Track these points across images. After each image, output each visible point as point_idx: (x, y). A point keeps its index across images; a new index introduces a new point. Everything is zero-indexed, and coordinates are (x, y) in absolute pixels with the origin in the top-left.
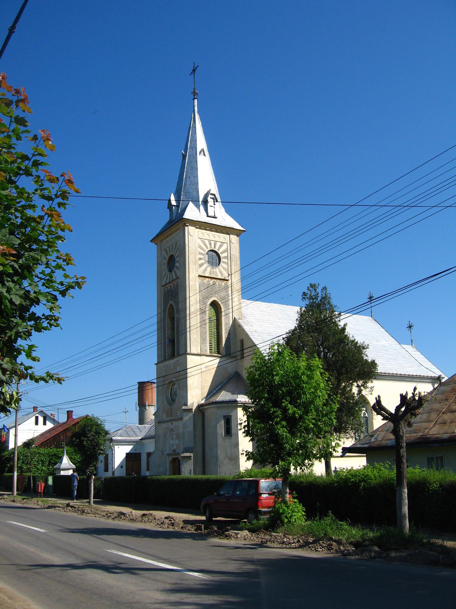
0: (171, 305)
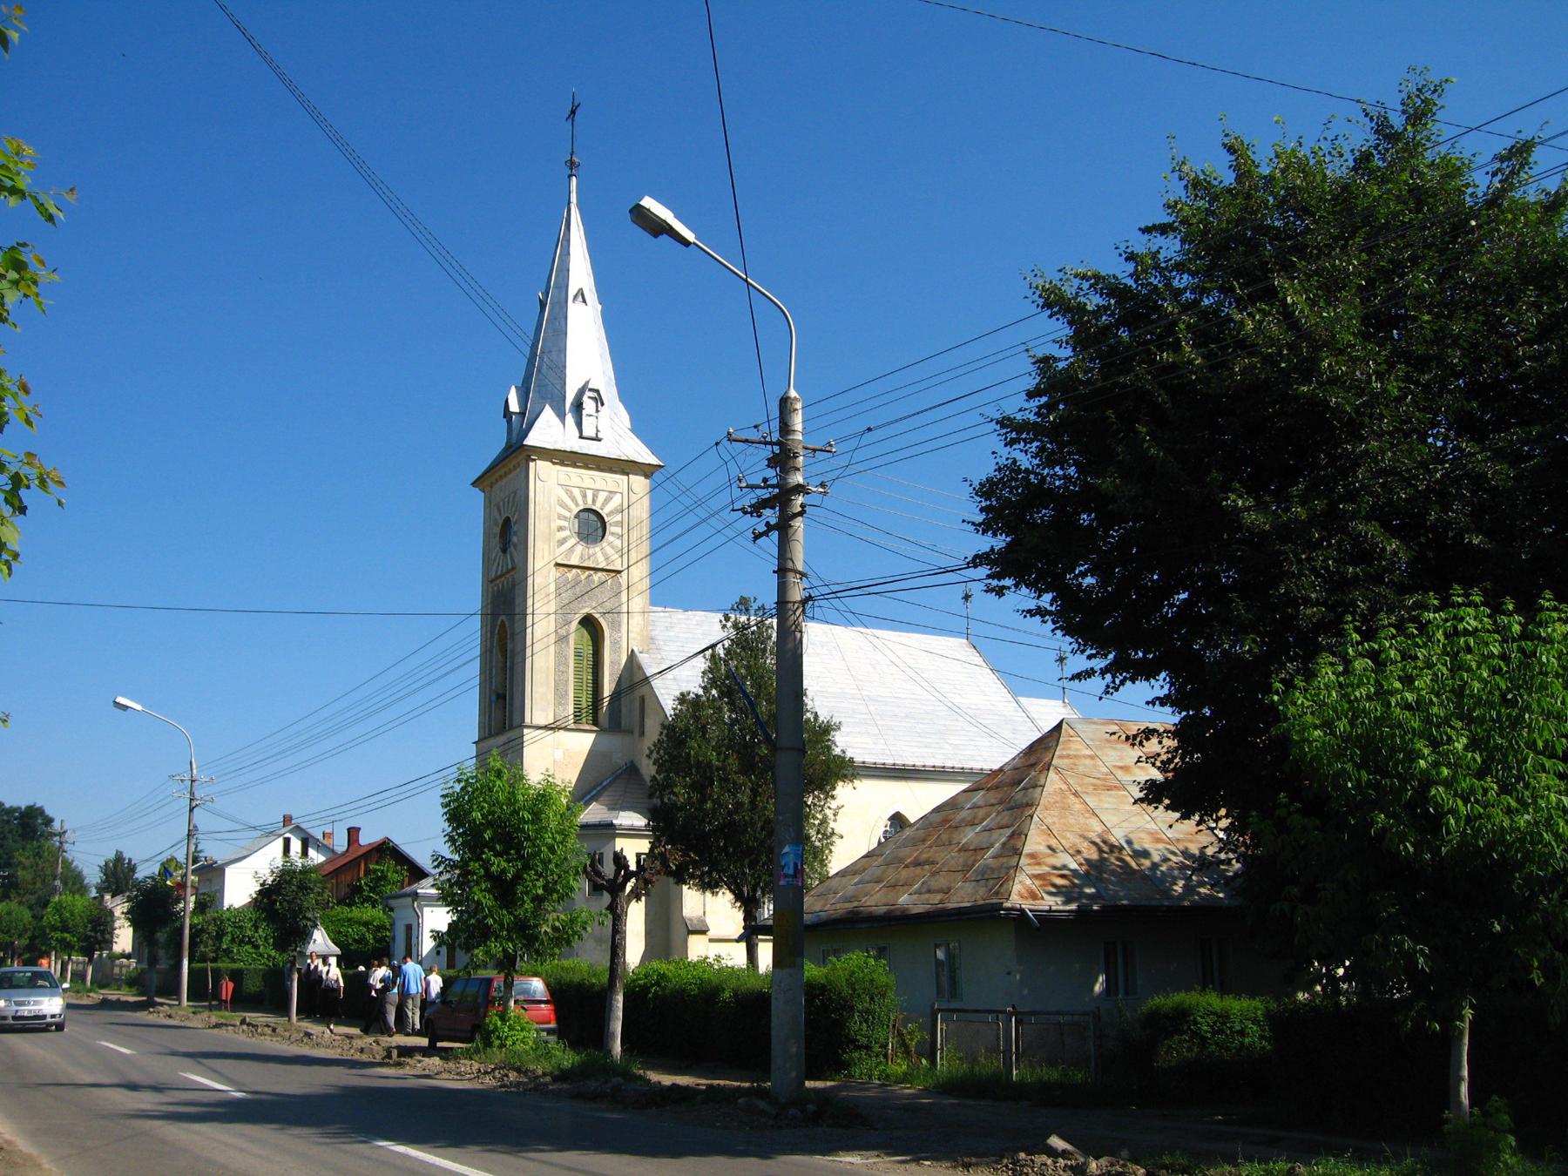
0: (503, 622)
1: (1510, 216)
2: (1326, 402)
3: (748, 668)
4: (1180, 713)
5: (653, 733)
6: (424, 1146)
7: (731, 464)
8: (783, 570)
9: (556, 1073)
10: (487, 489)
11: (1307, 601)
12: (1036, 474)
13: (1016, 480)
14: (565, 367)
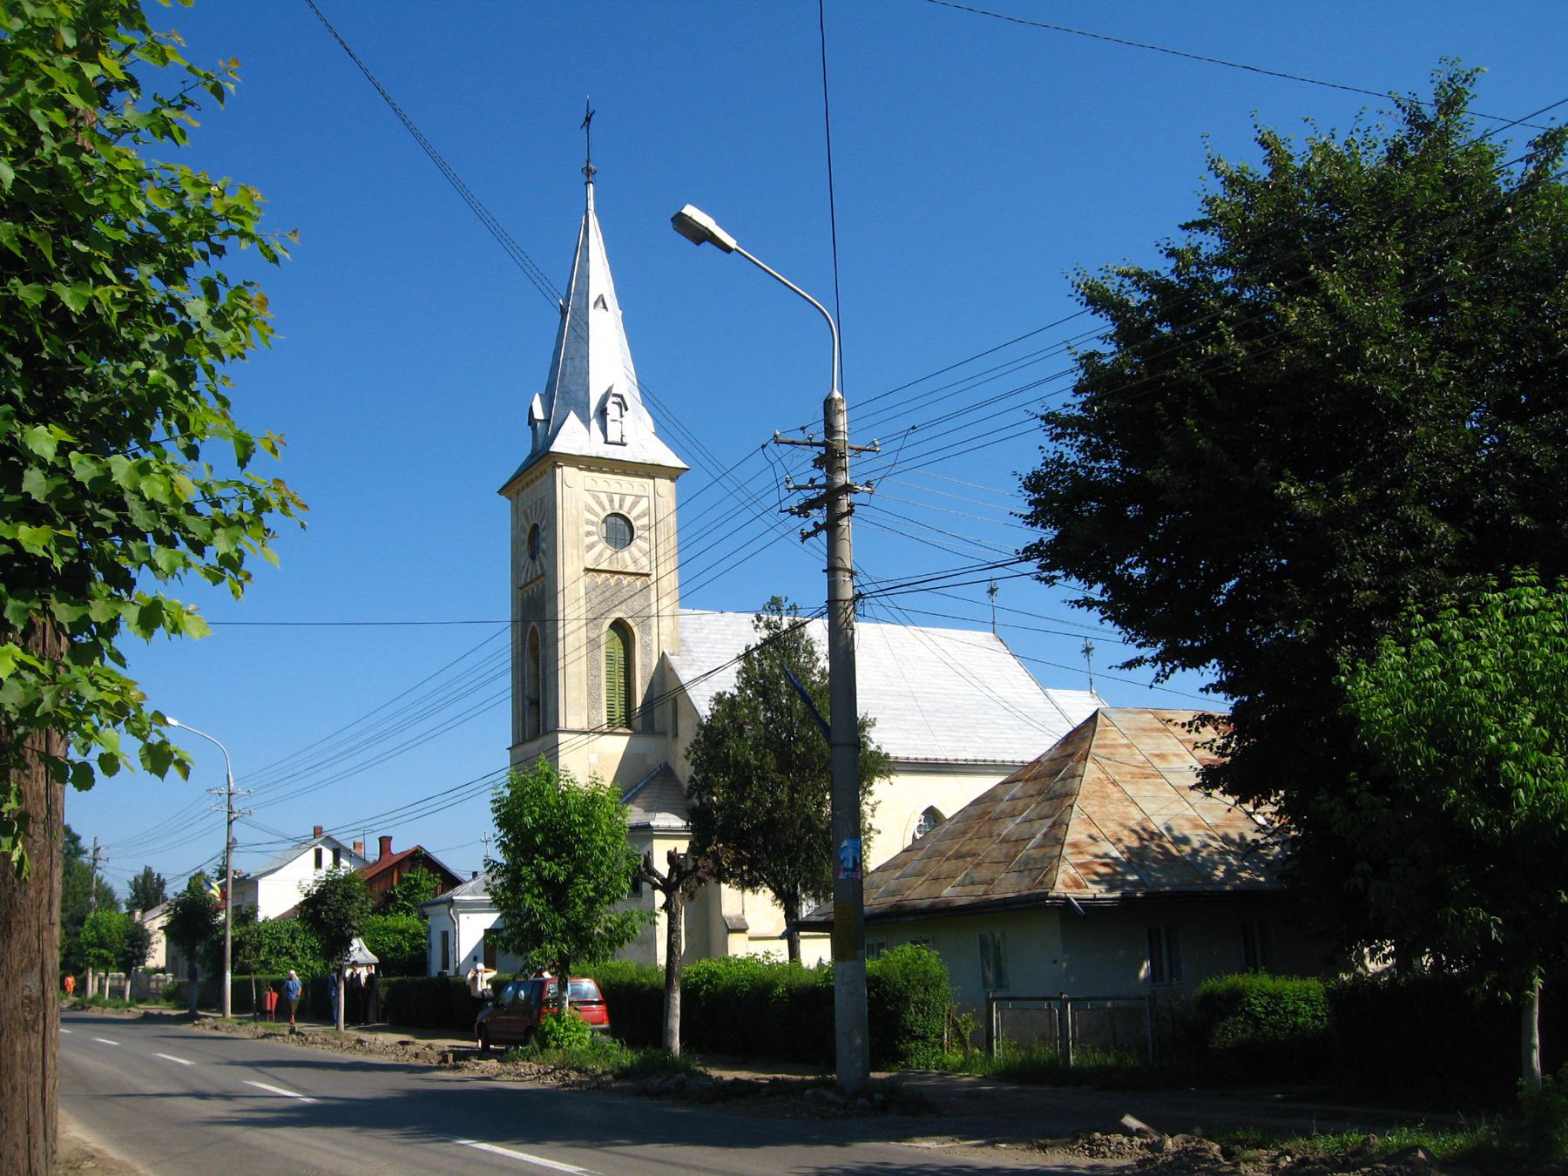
1: (1545, 202)
2: (1372, 390)
3: (781, 666)
4: (1232, 699)
5: (687, 734)
6: (504, 1143)
7: (778, 465)
9: (616, 1071)
11: (1360, 585)
12: (1084, 467)
13: (1063, 474)
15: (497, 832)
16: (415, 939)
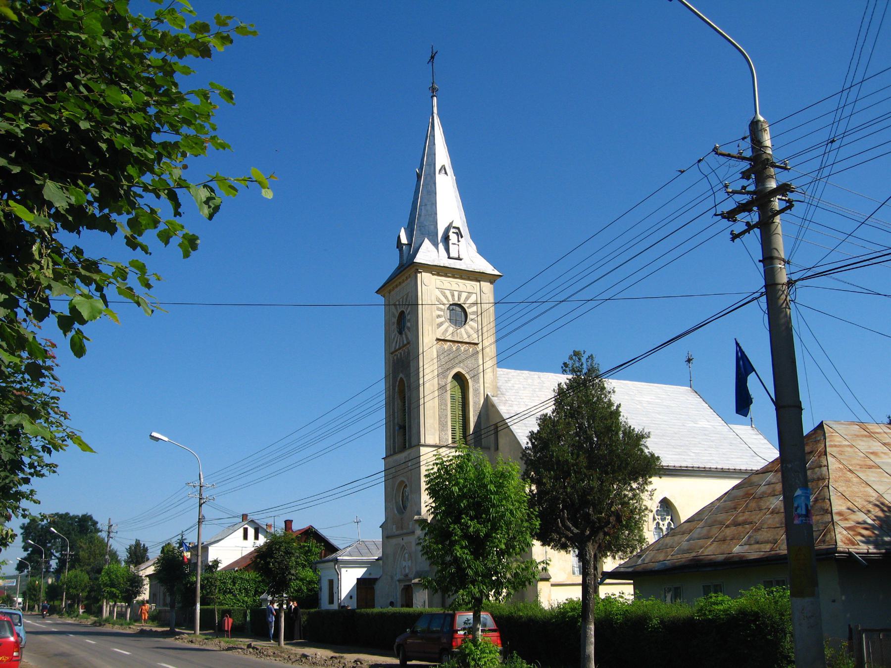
8: (768, 258)
10: (387, 295)
14: (436, 214)
15: (427, 500)
16: (310, 584)
